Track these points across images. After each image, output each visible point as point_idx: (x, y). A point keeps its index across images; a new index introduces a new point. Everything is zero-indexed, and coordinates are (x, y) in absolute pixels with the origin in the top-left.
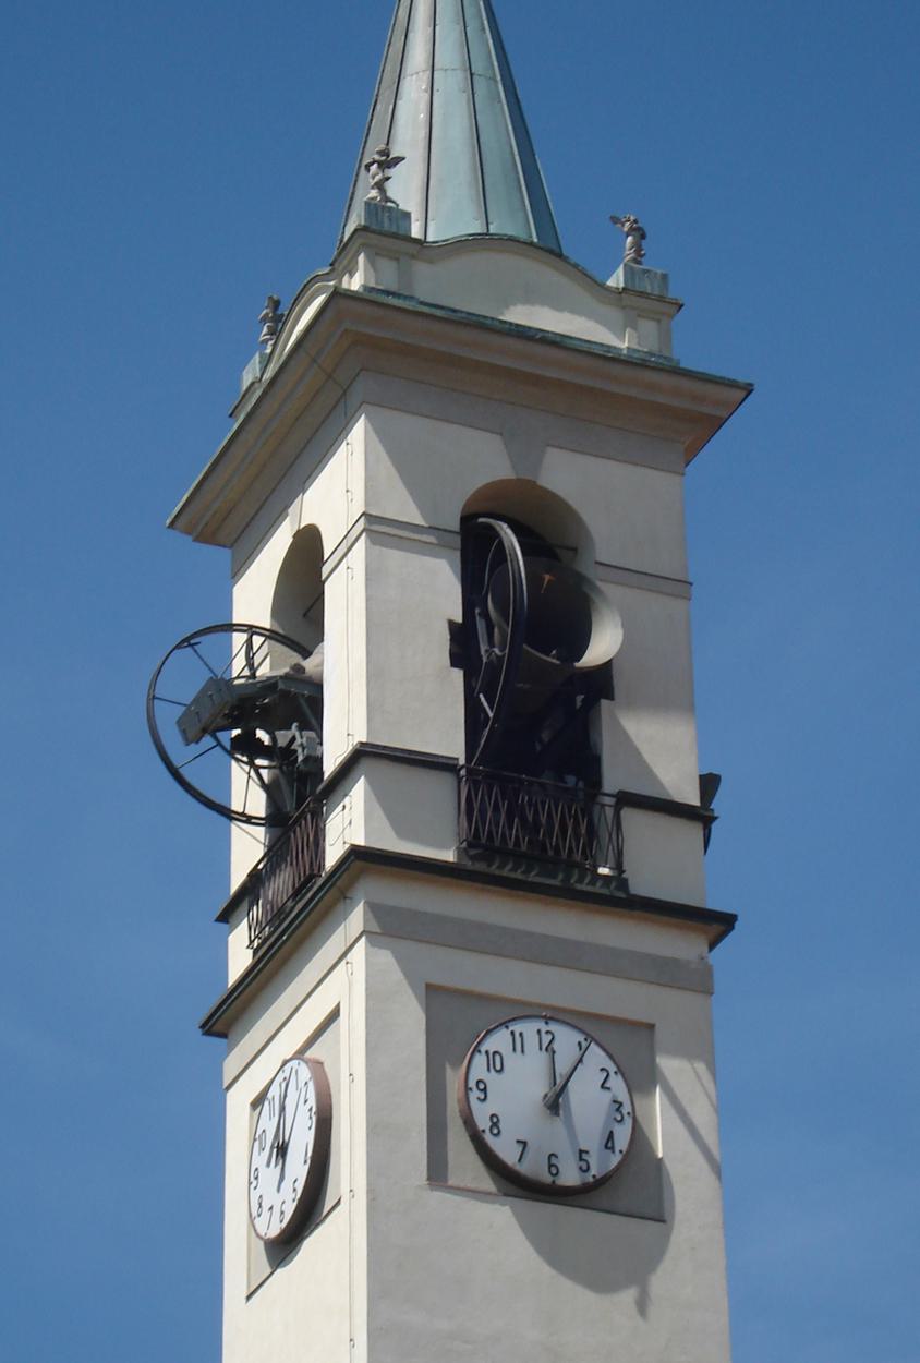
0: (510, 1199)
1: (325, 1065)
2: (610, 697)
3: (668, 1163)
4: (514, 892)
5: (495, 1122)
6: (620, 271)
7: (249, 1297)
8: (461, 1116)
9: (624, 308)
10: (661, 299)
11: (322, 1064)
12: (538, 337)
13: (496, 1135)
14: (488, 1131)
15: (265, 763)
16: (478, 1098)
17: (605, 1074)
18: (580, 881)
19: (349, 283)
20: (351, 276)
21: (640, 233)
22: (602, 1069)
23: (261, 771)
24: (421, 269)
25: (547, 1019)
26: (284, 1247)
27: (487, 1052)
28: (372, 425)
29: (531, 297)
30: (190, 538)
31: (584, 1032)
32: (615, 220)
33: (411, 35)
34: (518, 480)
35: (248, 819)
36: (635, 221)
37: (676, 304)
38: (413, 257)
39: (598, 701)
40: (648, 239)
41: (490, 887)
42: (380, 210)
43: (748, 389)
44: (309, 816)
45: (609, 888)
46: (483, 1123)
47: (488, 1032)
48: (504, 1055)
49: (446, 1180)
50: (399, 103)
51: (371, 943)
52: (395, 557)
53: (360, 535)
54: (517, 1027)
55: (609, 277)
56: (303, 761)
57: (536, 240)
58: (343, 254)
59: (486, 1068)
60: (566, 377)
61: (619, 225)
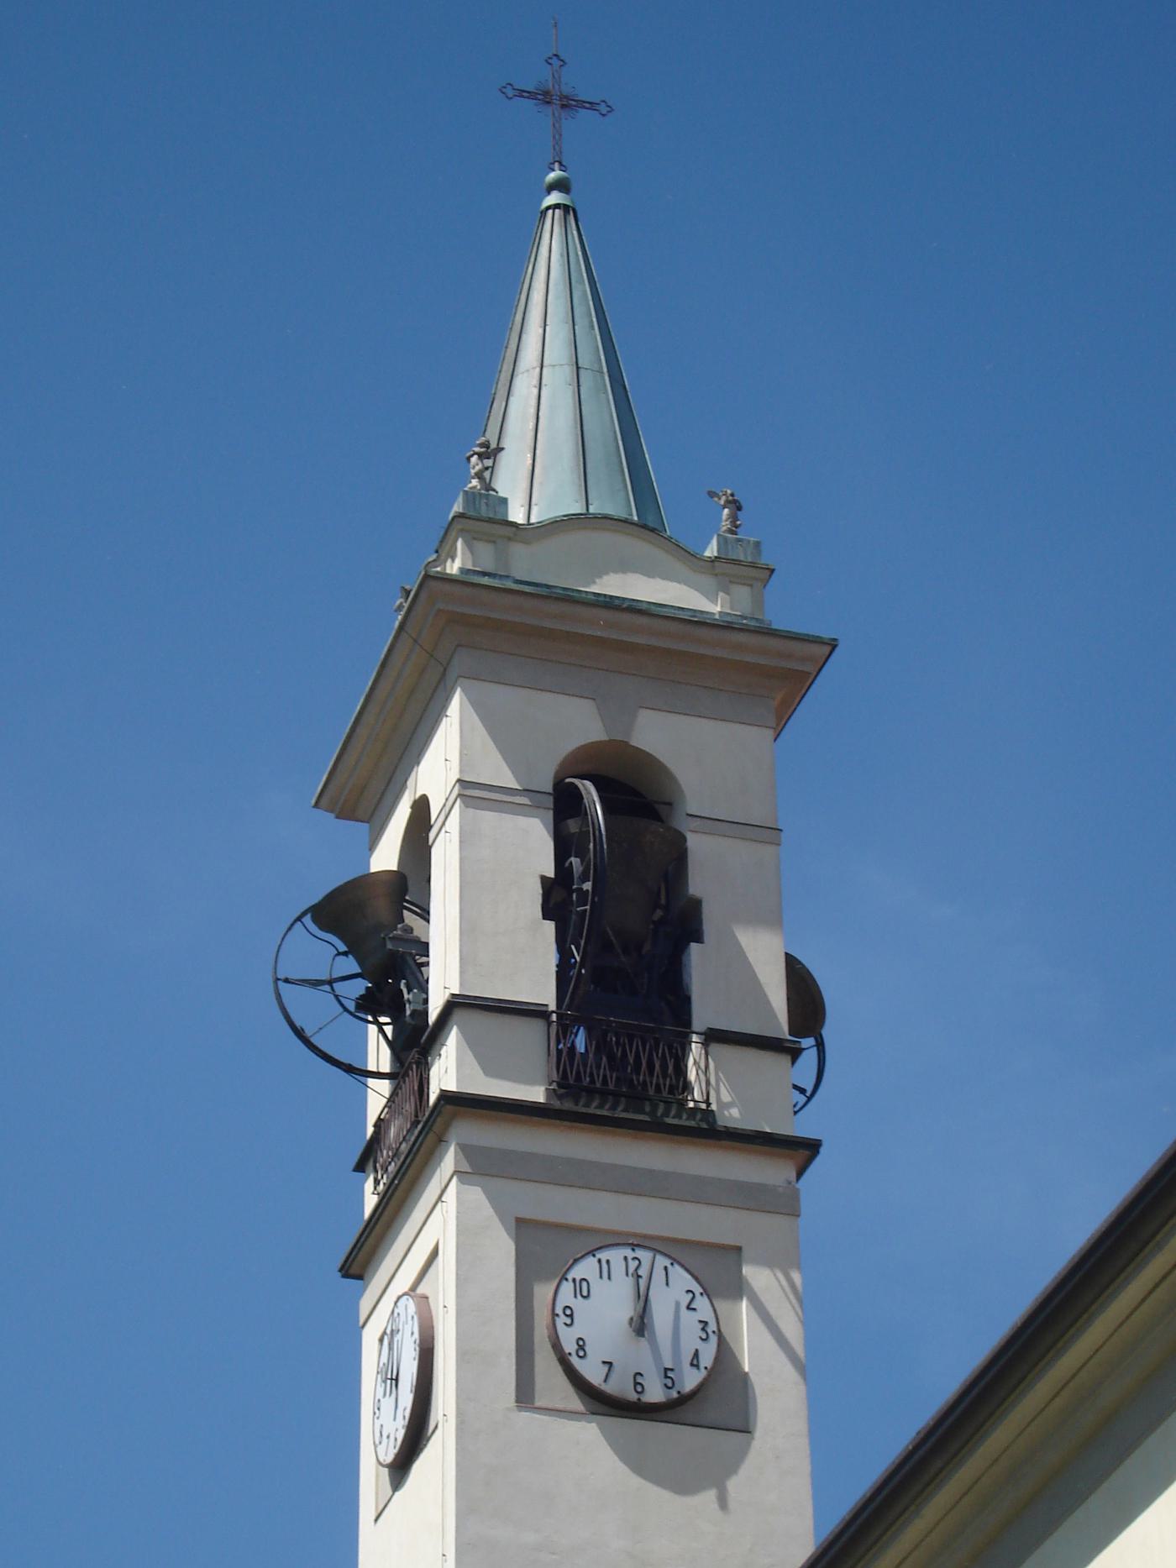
0: (599, 1417)
1: (430, 1300)
2: (699, 939)
3: (752, 1377)
4: (675, 1137)
5: (581, 1345)
6: (714, 542)
7: (376, 1520)
8: (550, 1341)
9: (716, 575)
10: (753, 565)
11: (427, 1298)
12: (625, 606)
13: (580, 1357)
14: (574, 1353)
15: (387, 1020)
16: (566, 1324)
17: (691, 1295)
18: (666, 1113)
19: (452, 567)
20: (453, 561)
21: (736, 505)
22: (688, 1291)
23: (385, 1027)
24: (518, 550)
25: (634, 1247)
26: (401, 1467)
27: (574, 1280)
28: (466, 695)
29: (624, 566)
30: (332, 816)
31: (669, 1257)
32: (712, 494)
33: (524, 337)
34: (610, 741)
35: (378, 1075)
36: (732, 495)
37: (768, 569)
38: (510, 539)
39: (688, 944)
40: (743, 511)
41: (582, 1125)
42: (478, 497)
43: (833, 645)
44: (414, 1066)
45: (681, 1118)
46: (569, 1347)
47: (576, 1261)
48: (589, 1281)
49: (533, 1404)
50: (511, 399)
51: (461, 1181)
52: (488, 818)
53: (454, 803)
54: (604, 1255)
55: (705, 549)
56: (410, 1015)
57: (636, 518)
58: (444, 545)
59: (573, 1295)
60: (654, 642)
61: (716, 499)
